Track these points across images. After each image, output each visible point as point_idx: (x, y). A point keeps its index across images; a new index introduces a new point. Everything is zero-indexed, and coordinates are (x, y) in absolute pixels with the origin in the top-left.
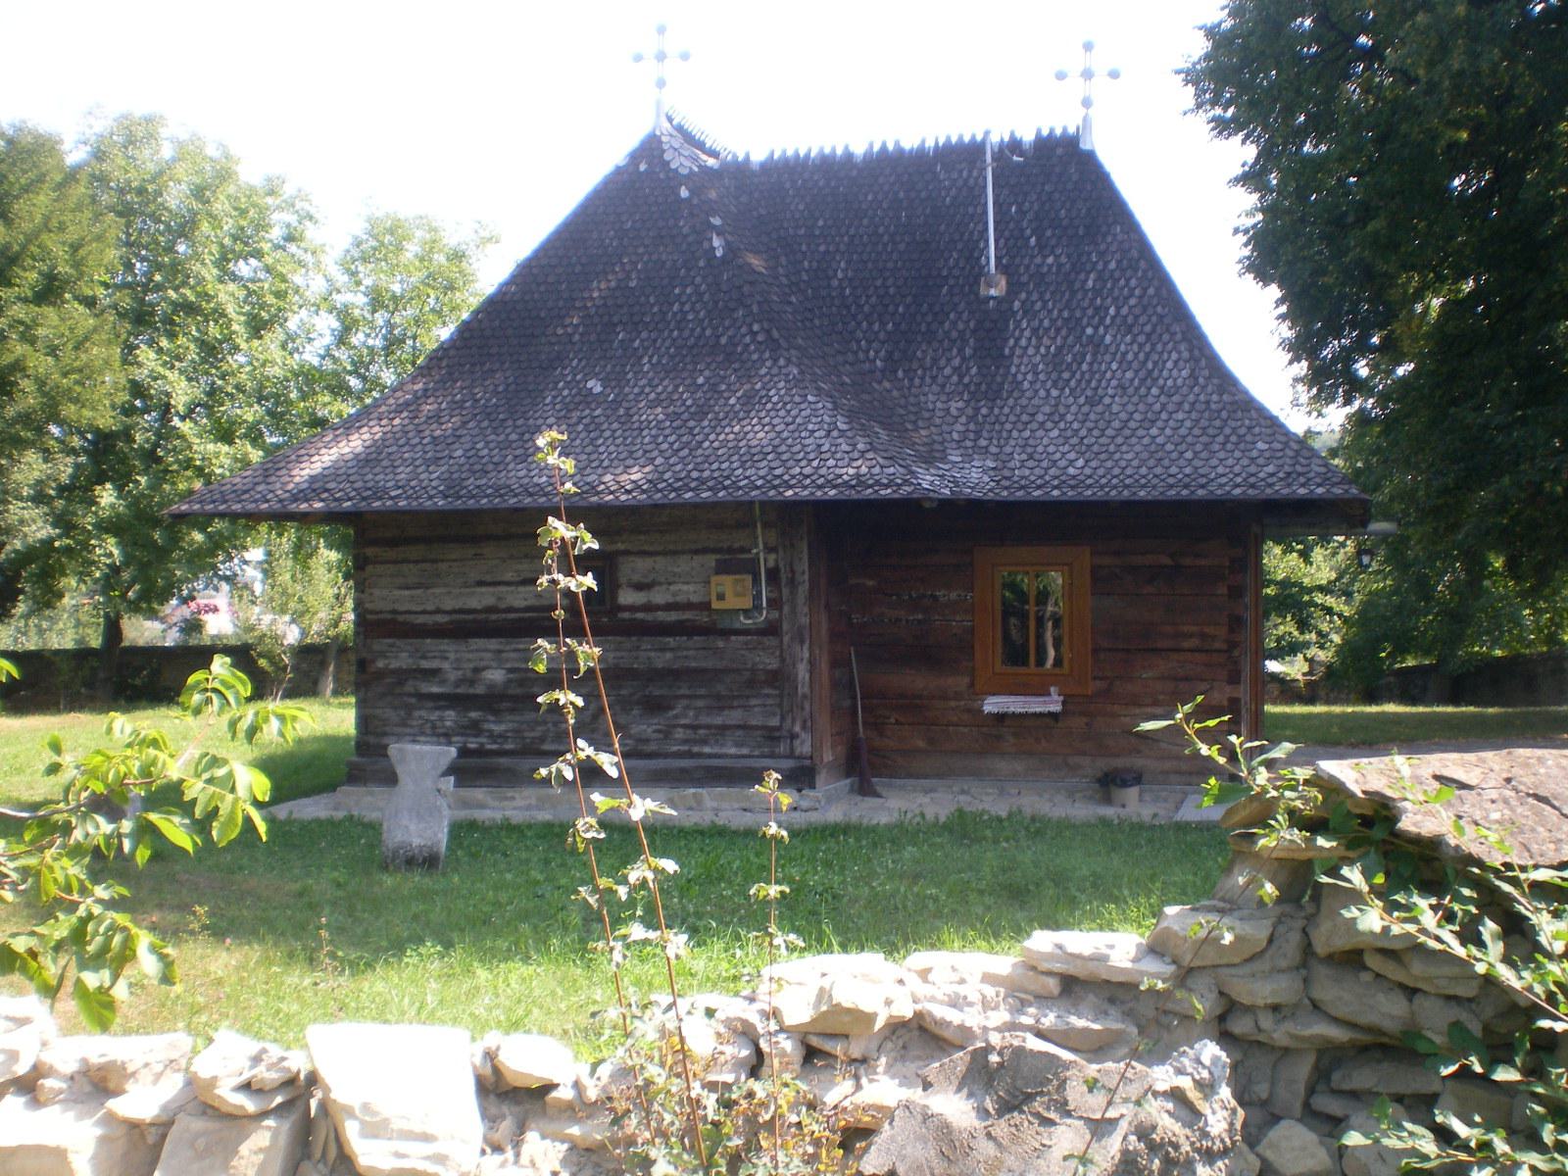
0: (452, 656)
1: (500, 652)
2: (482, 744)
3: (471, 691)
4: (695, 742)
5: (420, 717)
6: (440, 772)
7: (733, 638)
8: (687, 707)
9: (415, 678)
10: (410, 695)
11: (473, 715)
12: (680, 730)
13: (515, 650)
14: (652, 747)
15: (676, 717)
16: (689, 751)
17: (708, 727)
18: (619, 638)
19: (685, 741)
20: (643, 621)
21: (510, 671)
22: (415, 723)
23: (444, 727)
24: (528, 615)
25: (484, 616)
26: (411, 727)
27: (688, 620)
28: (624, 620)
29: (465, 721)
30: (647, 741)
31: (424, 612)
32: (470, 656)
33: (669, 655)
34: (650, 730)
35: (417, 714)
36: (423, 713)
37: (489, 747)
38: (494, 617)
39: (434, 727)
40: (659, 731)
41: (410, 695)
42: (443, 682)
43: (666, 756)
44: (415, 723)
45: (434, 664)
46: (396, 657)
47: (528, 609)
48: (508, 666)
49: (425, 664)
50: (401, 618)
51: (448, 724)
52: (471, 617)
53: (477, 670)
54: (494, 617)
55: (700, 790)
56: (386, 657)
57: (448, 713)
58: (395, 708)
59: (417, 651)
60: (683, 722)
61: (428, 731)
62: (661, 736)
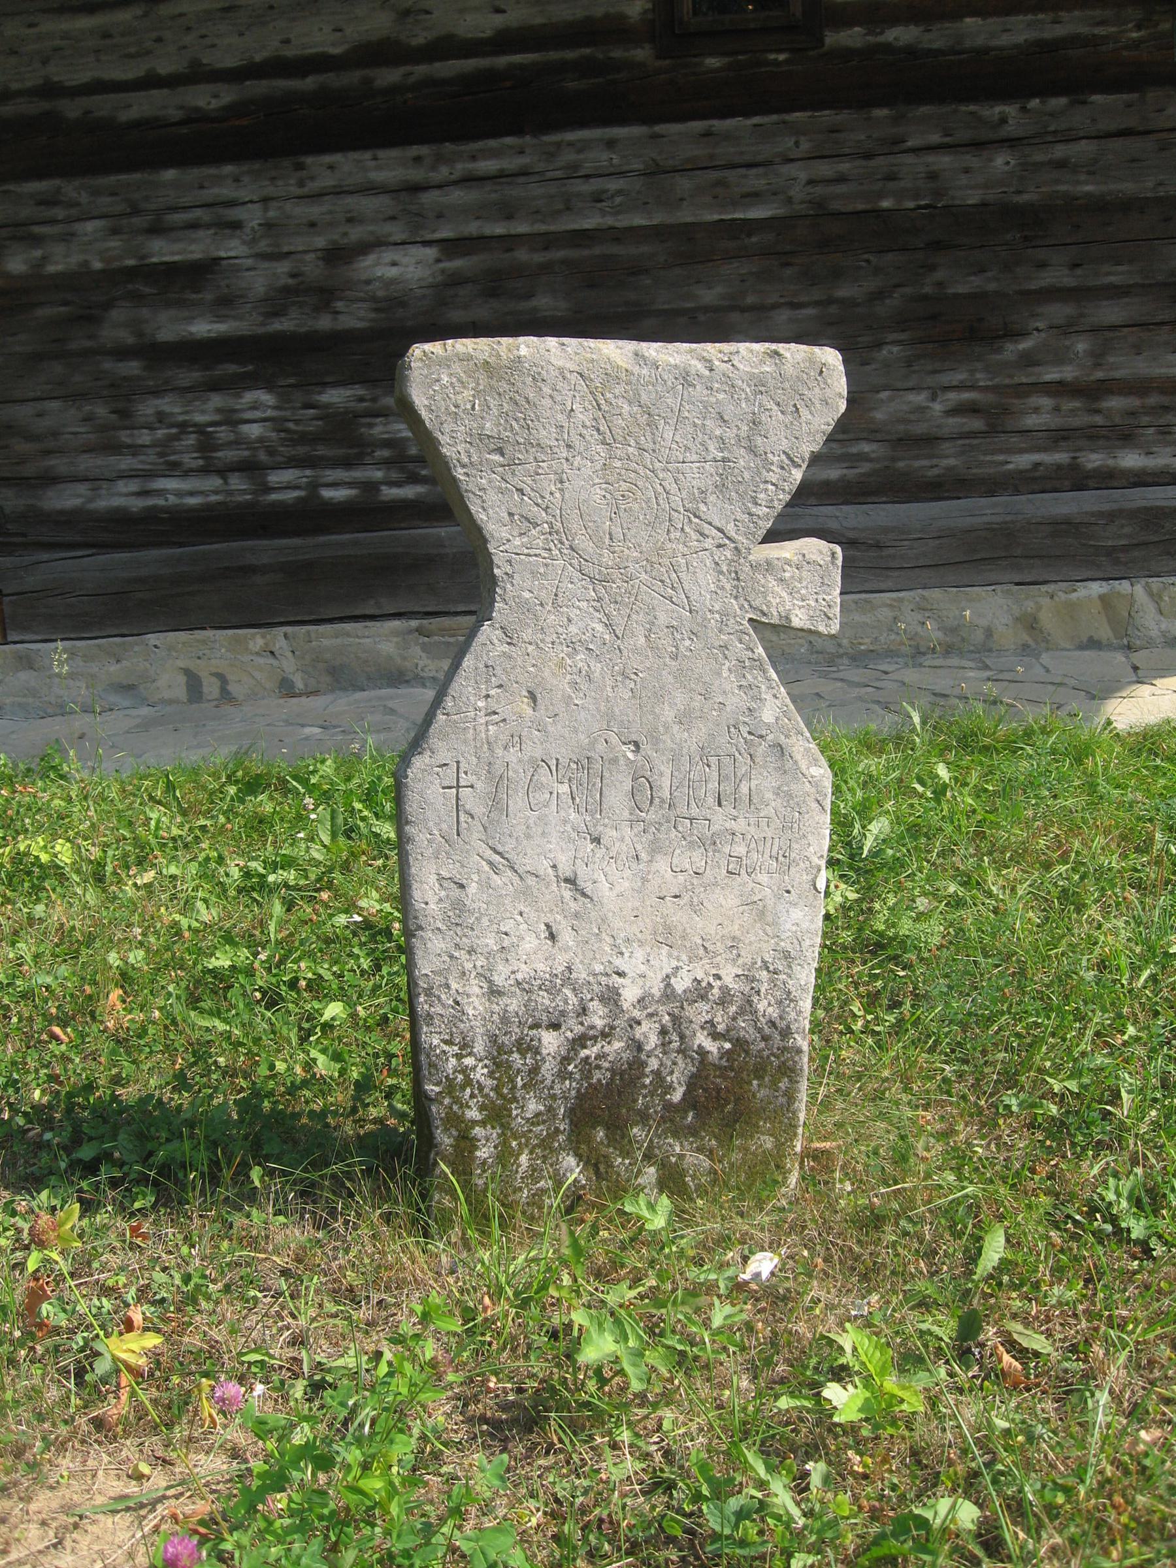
0: (252, 217)
1: (416, 188)
2: (370, 487)
3: (324, 323)
4: (1093, 436)
5: (161, 418)
6: (767, 511)
8: (1066, 329)
9: (138, 298)
10: (122, 353)
11: (335, 397)
12: (1046, 402)
13: (469, 180)
14: (949, 460)
15: (1028, 360)
16: (1074, 466)
17: (1138, 387)
18: (827, 116)
19: (1059, 437)
20: (910, 52)
21: (451, 247)
22: (145, 437)
23: (237, 443)
24: (502, 61)
25: (352, 78)
26: (135, 450)
27: (1074, 40)
28: (847, 54)
29: (308, 421)
30: (928, 441)
31: (151, 82)
32: (314, 211)
33: (1002, 161)
34: (937, 407)
35: (147, 408)
36: (169, 405)
37: (391, 493)
38: (389, 76)
39: (207, 445)
40: (972, 409)
41: (122, 353)
42: (225, 303)
43: (993, 486)
44: (145, 437)
45: (195, 248)
46: (67, 238)
47: (504, 41)
48: (445, 233)
49: (163, 251)
50: (72, 109)
51: (254, 431)
52: (309, 83)
53: (337, 255)
54: (389, 76)
55: (1124, 586)
56: (36, 240)
57: (249, 397)
58: (76, 397)
59: (136, 211)
60: (1051, 375)
61: (190, 460)
62: (977, 424)
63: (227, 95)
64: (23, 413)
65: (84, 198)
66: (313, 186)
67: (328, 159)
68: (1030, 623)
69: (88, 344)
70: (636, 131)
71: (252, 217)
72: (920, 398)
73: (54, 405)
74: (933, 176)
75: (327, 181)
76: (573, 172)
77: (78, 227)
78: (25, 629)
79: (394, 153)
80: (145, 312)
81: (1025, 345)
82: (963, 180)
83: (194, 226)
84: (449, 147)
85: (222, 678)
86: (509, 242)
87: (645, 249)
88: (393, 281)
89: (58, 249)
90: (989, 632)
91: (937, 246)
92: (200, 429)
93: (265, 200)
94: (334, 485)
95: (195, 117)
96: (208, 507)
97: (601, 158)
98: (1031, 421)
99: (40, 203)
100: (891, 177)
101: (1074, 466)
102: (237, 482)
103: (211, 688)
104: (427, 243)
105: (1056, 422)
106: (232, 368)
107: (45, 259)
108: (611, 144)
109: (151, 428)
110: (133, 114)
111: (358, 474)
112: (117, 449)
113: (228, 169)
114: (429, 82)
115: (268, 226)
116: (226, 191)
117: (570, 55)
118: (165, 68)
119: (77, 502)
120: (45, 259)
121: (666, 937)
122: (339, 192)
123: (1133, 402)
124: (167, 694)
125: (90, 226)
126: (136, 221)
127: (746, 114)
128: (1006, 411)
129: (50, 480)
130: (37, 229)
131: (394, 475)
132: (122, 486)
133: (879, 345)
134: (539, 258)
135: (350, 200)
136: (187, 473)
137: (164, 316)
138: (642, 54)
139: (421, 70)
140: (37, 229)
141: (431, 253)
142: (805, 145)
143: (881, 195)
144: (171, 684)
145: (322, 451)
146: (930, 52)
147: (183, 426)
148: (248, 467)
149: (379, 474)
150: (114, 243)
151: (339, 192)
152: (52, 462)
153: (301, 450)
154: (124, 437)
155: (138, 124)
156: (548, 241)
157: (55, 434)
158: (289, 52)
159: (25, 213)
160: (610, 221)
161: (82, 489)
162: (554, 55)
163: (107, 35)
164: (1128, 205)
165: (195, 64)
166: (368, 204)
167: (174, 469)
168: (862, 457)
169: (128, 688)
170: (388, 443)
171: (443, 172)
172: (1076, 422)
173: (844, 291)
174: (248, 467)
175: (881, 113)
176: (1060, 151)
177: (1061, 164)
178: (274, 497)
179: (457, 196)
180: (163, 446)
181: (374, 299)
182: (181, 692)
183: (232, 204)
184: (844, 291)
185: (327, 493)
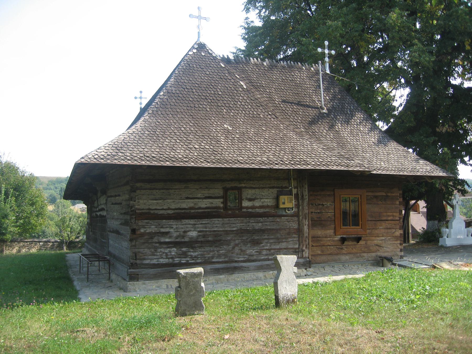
0: (175, 227)
2: (188, 261)
3: (183, 240)
4: (270, 255)
5: (161, 251)
7: (283, 218)
8: (267, 243)
9: (159, 236)
10: (156, 243)
11: (184, 249)
12: (265, 251)
13: (201, 224)
14: (255, 258)
15: (263, 246)
16: (268, 258)
17: (274, 249)
19: (267, 255)
20: (251, 212)
21: (199, 232)
24: (206, 210)
26: (157, 255)
27: (267, 212)
28: (244, 212)
30: (252, 255)
32: (183, 226)
33: (260, 224)
34: (254, 252)
35: (159, 250)
36: (162, 250)
37: (190, 261)
38: (193, 211)
39: (167, 255)
40: (257, 252)
41: (156, 243)
42: (170, 237)
43: (260, 260)
44: (158, 254)
45: (167, 230)
47: (207, 208)
48: (198, 230)
49: (162, 230)
50: (152, 212)
51: (173, 253)
52: (183, 211)
53: (185, 232)
54: (193, 211)
56: (145, 228)
57: (173, 249)
58: (149, 248)
59: (159, 225)
61: (164, 257)
62: (258, 253)
63: (173, 212)
64: (141, 250)
65: (152, 223)
66: (182, 223)
67: (185, 220)
68: (265, 276)
69: (151, 241)
70: (221, 219)
71: (175, 227)
72: (252, 250)
73: (146, 249)
74: (253, 226)
75: (184, 223)
76: (214, 223)
77: (151, 226)
78: (141, 279)
79: (193, 220)
80: (160, 238)
81: (263, 245)
82: (256, 226)
83: (167, 227)
84: (199, 220)
85: (171, 285)
86: (206, 231)
87: (222, 233)
88: (191, 236)
89: (148, 229)
90: (261, 277)
91: (254, 233)
92: (166, 253)
93: (176, 225)
94: (183, 260)
95: (168, 214)
96: (166, 263)
97: (217, 222)
98: (263, 253)
99: (146, 223)
100: (249, 226)
101: (268, 258)
102: (170, 260)
103: (170, 287)
104: (196, 231)
105: (266, 253)
106: (171, 245)
107: (146, 230)
108: (218, 220)
109: (159, 253)
110: (160, 213)
111: (186, 259)
112: (155, 255)
113: (172, 221)
114: (197, 212)
115: (176, 228)
116: (171, 223)
117: (214, 210)
118: (165, 208)
119: (148, 262)
120: (146, 230)
121: (290, 291)
122: (186, 224)
123: (274, 251)
124: (164, 288)
125: (153, 226)
126: (159, 226)
127: (233, 218)
128: (261, 252)
129: (145, 259)
130: (146, 226)
131: (191, 259)
132: (155, 260)
133: (247, 244)
134: (209, 233)
135: (187, 225)
136: (164, 259)
137: (162, 238)
138: (222, 211)
139: (197, 211)
140: (146, 226)
141: (197, 232)
142: (240, 222)
143: (247, 228)
144: (165, 286)
145: (182, 256)
146: (253, 212)
147: (164, 253)
148: (172, 258)
149: (189, 259)
150: (156, 229)
151: (186, 224)
152: (145, 257)
153: (179, 256)
154: (156, 254)
155: (160, 214)
156: (210, 231)
157: (146, 253)
158: (180, 207)
159: (144, 224)
160: (218, 229)
161: (149, 260)
162: (212, 210)
163: (158, 203)
164: (273, 229)
165: (169, 208)
166: (189, 226)
167: (162, 258)
168: (245, 257)
169: (158, 287)
170: (190, 255)
171: (198, 223)
172: (268, 253)
173: (243, 238)
174: (172, 258)
175: (247, 218)
176: (266, 223)
177: (266, 225)
178: (175, 262)
179: (200, 226)
180: (161, 255)
181: (189, 237)
182: (166, 287)
183: (172, 225)
184: (243, 238)
185: (182, 261)
